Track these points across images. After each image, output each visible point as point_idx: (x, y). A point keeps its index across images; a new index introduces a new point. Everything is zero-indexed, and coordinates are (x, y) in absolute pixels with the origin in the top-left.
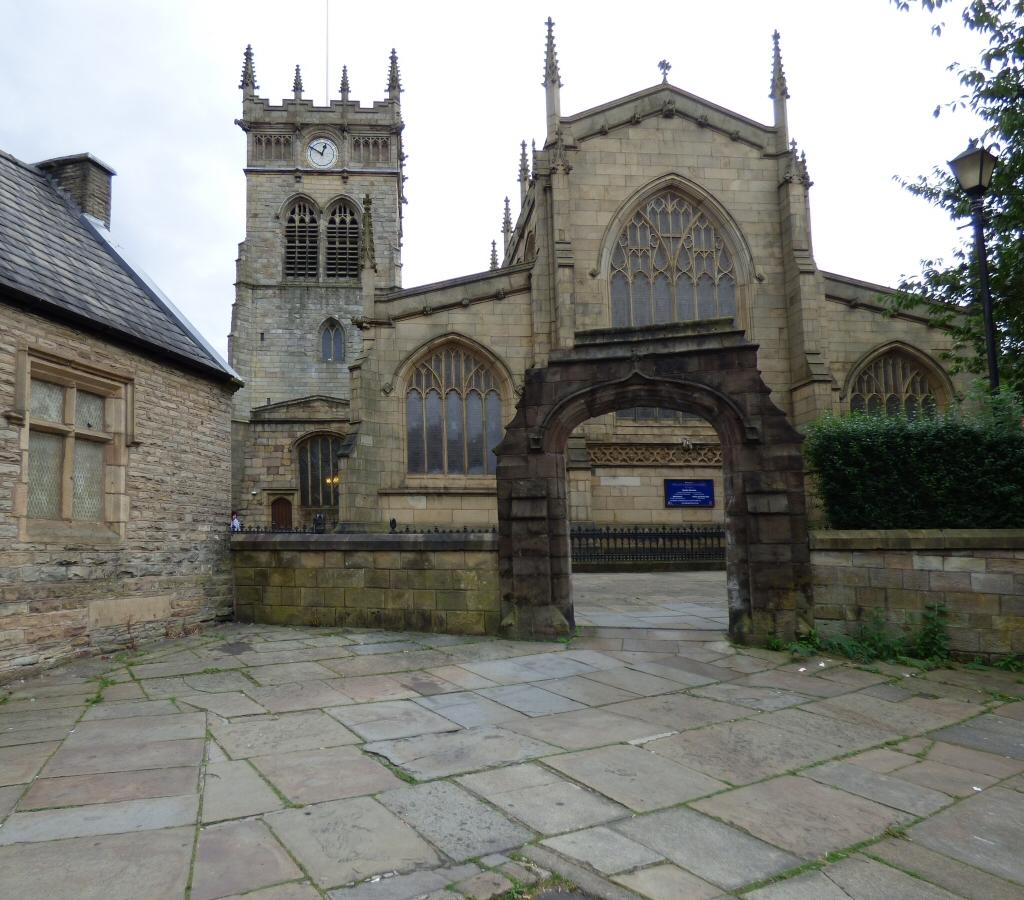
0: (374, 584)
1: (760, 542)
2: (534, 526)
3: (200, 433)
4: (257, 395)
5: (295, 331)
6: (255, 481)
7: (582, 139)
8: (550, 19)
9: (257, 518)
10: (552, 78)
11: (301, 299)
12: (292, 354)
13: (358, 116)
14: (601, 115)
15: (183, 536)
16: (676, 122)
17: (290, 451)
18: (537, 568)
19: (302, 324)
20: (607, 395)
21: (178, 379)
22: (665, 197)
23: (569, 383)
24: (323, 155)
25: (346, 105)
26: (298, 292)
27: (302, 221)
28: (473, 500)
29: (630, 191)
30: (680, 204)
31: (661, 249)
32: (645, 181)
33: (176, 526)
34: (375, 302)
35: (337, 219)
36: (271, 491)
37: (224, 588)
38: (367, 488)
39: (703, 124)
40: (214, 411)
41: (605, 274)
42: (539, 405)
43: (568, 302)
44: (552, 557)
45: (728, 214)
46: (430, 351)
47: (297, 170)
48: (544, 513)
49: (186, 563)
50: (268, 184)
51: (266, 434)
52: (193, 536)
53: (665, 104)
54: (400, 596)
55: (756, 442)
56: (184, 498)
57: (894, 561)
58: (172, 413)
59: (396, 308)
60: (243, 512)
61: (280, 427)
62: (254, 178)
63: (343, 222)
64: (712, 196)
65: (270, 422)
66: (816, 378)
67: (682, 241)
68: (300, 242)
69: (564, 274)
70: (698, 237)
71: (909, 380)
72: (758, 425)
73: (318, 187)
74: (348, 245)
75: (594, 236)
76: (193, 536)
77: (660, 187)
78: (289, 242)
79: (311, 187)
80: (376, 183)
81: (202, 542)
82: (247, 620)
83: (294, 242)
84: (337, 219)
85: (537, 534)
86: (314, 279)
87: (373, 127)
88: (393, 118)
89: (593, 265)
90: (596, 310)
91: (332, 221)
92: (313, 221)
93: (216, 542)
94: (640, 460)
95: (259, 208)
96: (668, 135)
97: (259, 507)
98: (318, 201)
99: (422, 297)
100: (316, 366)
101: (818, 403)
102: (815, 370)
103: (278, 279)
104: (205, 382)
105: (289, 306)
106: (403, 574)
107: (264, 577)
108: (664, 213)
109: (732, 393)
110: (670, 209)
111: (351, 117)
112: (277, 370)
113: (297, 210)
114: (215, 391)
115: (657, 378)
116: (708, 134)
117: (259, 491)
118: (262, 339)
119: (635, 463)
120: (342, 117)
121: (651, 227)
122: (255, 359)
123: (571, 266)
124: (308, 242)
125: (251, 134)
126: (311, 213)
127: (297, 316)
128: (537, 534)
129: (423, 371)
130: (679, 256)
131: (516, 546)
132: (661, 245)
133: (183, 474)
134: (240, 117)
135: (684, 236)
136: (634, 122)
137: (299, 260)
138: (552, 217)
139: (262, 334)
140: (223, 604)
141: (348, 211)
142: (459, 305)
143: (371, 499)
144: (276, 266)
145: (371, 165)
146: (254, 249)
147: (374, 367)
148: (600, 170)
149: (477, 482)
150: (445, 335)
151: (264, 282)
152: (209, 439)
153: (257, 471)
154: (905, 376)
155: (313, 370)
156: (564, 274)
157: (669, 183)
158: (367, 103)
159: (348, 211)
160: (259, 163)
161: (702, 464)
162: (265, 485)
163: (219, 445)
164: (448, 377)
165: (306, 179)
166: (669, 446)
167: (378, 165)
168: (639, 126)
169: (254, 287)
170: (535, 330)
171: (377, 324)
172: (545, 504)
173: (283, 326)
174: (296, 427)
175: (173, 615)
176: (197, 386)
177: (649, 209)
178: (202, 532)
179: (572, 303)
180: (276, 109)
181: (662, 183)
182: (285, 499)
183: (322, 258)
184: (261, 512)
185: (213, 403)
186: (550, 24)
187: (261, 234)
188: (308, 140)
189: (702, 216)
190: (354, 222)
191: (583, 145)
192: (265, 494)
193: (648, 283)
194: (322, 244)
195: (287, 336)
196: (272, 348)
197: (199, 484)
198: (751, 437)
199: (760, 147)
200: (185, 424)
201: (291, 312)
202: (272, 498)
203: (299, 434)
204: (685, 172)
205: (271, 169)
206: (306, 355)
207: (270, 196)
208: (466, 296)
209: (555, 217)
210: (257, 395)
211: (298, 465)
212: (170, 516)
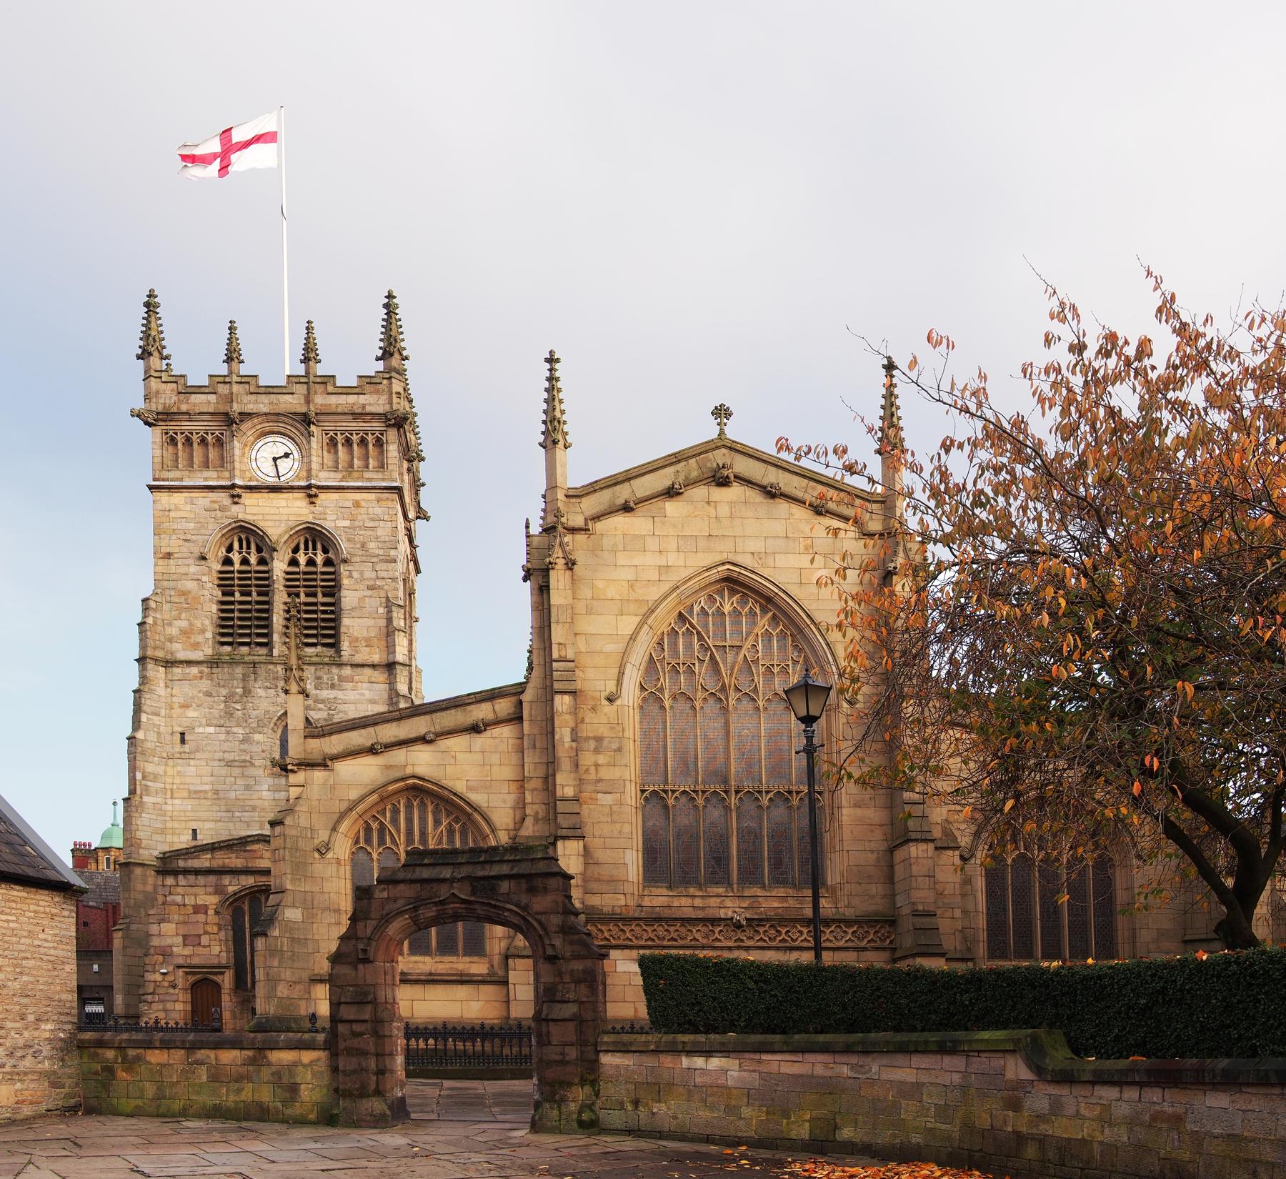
0: (215, 1077)
1: (549, 1044)
2: (357, 1028)
3: (41, 940)
4: (176, 825)
5: (235, 730)
6: (166, 953)
7: (597, 518)
9: (169, 1006)
10: (527, 527)
11: (244, 680)
12: (229, 764)
13: (333, 400)
14: (626, 485)
15: (26, 1034)
16: (736, 491)
17: (217, 913)
18: (360, 1064)
19: (246, 718)
20: (430, 912)
21: (17, 892)
23: (395, 900)
26: (239, 671)
27: (245, 561)
29: (666, 587)
32: (685, 574)
33: (18, 1025)
34: (305, 737)
35: (302, 559)
36: (190, 969)
37: (68, 1082)
38: (293, 973)
40: (56, 918)
41: (631, 694)
42: (367, 918)
43: (567, 738)
44: (377, 1055)
45: (809, 616)
46: (382, 800)
47: (233, 486)
48: (367, 1017)
49: (29, 1058)
50: (188, 507)
51: (180, 890)
52: (36, 1034)
53: (719, 468)
54: (239, 1091)
55: (556, 957)
56: (26, 1000)
57: (667, 1060)
58: (12, 925)
59: (335, 744)
60: (149, 998)
61: (201, 880)
62: (164, 497)
63: (311, 562)
64: (785, 592)
65: (186, 872)
66: (913, 836)
67: (744, 651)
68: (242, 594)
70: (768, 646)
72: (558, 942)
73: (267, 510)
74: (320, 599)
75: (615, 647)
76: (36, 1034)
77: (712, 579)
78: (224, 594)
79: (255, 509)
80: (363, 504)
81: (47, 1039)
82: (90, 1111)
83: (232, 594)
84: (302, 559)
85: (360, 1034)
86: (263, 651)
87: (358, 416)
88: (391, 403)
89: (611, 687)
90: (615, 746)
91: (294, 562)
93: (61, 1040)
94: (673, 939)
95: (172, 544)
96: (724, 510)
97: (172, 991)
98: (270, 531)
99: (371, 730)
100: (270, 781)
101: (914, 868)
103: (207, 651)
104: (47, 892)
105: (224, 692)
106: (244, 1070)
107: (110, 1070)
109: (537, 913)
110: (727, 608)
111: (320, 400)
112: (207, 787)
113: (236, 546)
114: (57, 899)
115: (472, 898)
116: (782, 506)
117: (171, 968)
118: (183, 741)
119: (665, 943)
120: (308, 402)
121: (698, 633)
122: (170, 771)
123: (573, 693)
124: (254, 594)
125: (158, 430)
126: (259, 550)
127: (238, 706)
128: (360, 1034)
129: (375, 826)
130: (740, 670)
131: (342, 1045)
132: (712, 657)
133: (25, 978)
134: (140, 404)
135: (748, 645)
136: (671, 493)
138: (550, 626)
139: (183, 734)
140: (68, 1096)
141: (319, 546)
142: (423, 740)
143: (298, 987)
144: (203, 631)
145: (355, 475)
146: (166, 607)
147: (304, 822)
148: (622, 559)
149: (448, 966)
150: (403, 779)
151: (181, 656)
152: (51, 945)
153: (169, 941)
155: (266, 787)
156: (562, 703)
157: (724, 575)
158: (347, 378)
159: (319, 546)
160: (171, 475)
161: (759, 944)
162: (181, 961)
163: (63, 950)
164: (410, 832)
165: (248, 498)
166: (714, 921)
167: (367, 475)
168: (680, 498)
169: (169, 663)
170: (526, 774)
172: (369, 1008)
173: (215, 722)
174: (226, 880)
175: (17, 1103)
176: (38, 897)
177: (696, 609)
178: (45, 1030)
179: (573, 741)
180: (198, 390)
181: (714, 575)
182: (211, 980)
184: (175, 998)
185: (54, 911)
187: (179, 585)
188: (251, 439)
189: (774, 617)
190: (328, 562)
191: (600, 526)
192: (181, 972)
193: (693, 708)
194: (276, 598)
195: (223, 737)
196: (198, 755)
197: (42, 987)
198: (550, 952)
200: (25, 934)
201: (228, 699)
202: (192, 979)
203: (231, 889)
205: (191, 483)
206: (252, 765)
207: (192, 525)
208: (433, 730)
209: (553, 626)
210: (176, 825)
211: (231, 933)
212: (12, 1016)
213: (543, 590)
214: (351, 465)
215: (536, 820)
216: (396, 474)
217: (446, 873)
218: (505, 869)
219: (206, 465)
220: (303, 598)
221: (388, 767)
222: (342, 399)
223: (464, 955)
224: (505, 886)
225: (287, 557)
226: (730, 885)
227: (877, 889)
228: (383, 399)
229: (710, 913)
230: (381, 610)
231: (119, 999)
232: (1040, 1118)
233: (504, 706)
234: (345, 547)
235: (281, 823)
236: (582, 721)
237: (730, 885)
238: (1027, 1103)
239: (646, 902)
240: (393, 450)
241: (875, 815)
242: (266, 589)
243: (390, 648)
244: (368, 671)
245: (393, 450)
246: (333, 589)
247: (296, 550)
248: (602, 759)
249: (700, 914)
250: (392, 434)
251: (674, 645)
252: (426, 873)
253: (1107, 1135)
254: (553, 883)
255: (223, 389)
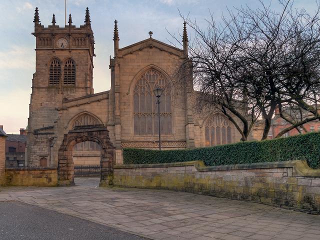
2: (64, 165)
6: (35, 153)
7: (125, 55)
8: (116, 20)
10: (116, 38)
13: (75, 31)
16: (154, 49)
22: (150, 71)
24: (62, 42)
25: (70, 27)
27: (55, 66)
28: (91, 158)
29: (139, 70)
30: (155, 73)
31: (149, 86)
32: (143, 67)
35: (68, 65)
36: (40, 156)
39: (161, 50)
59: (68, 105)
62: (38, 52)
63: (70, 66)
65: (40, 134)
69: (117, 95)
70: (160, 82)
71: (223, 122)
79: (58, 54)
84: (68, 65)
87: (80, 34)
89: (127, 91)
90: (128, 104)
91: (66, 66)
92: (59, 66)
98: (61, 59)
102: (189, 120)
107: (12, 176)
108: (150, 76)
110: (152, 74)
111: (72, 31)
118: (41, 105)
126: (59, 63)
135: (156, 82)
136: (140, 50)
137: (54, 78)
144: (46, 81)
154: (222, 121)
156: (117, 95)
158: (78, 26)
162: (38, 154)
165: (56, 52)
171: (63, 109)
174: (48, 135)
180: (46, 29)
183: (62, 77)
186: (116, 22)
190: (73, 66)
191: (125, 57)
198: (104, 147)
199: (178, 56)
204: (156, 64)
213: (113, 71)
214: (78, 45)
215: (111, 120)
216: (88, 47)
217: (82, 131)
218: (95, 129)
219: (48, 45)
220: (68, 73)
221: (80, 109)
222: (77, 30)
223: (97, 150)
224: (94, 133)
225: (65, 65)
226: (152, 134)
227: (183, 134)
228: (85, 30)
229: (148, 140)
230: (84, 76)
231: (26, 163)
232: (198, 179)
233: (105, 96)
234: (77, 62)
235: (57, 122)
236: (121, 99)
237: (152, 134)
238: (196, 177)
239: (135, 138)
240: (87, 41)
241: (182, 118)
242: (60, 71)
243: (86, 84)
244: (81, 89)
245: (87, 41)
246: (74, 72)
247: (66, 63)
248: (125, 107)
249: (146, 141)
250: (87, 38)
251: (141, 83)
252: (78, 131)
253: (210, 183)
254: (104, 132)
255: (51, 28)
